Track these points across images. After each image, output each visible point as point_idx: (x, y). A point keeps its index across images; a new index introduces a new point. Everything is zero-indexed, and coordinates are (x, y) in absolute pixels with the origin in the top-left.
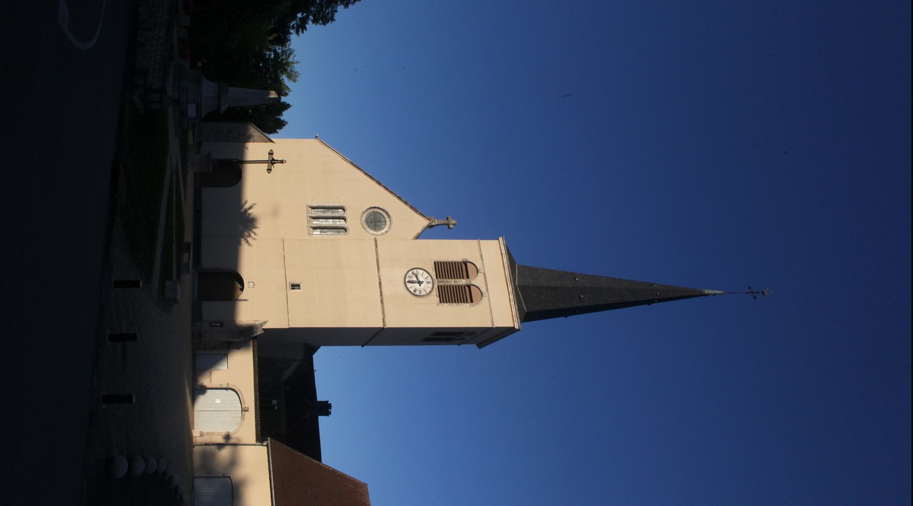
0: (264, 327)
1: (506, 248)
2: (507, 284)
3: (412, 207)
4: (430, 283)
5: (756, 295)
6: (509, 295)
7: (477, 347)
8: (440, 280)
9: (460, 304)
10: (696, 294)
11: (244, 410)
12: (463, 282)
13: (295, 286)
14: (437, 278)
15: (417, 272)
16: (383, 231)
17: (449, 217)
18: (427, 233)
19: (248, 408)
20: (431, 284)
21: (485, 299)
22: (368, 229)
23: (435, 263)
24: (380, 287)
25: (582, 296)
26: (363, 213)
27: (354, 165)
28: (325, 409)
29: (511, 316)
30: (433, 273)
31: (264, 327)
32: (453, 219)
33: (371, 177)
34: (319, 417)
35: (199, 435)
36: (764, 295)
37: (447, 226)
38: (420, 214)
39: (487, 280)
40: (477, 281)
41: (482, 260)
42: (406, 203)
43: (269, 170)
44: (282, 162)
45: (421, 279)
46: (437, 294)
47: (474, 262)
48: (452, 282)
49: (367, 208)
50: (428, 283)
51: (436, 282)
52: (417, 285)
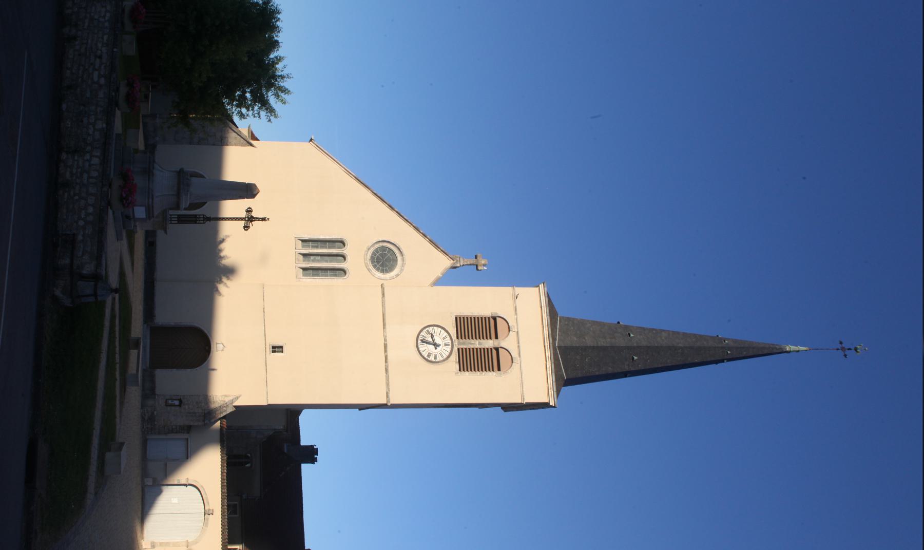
0: (234, 404)
1: (547, 298)
2: (545, 347)
3: (431, 241)
4: (449, 345)
5: (847, 352)
6: (546, 361)
7: (501, 410)
8: (461, 341)
9: (484, 373)
10: (775, 351)
11: (207, 513)
12: (489, 343)
13: (277, 349)
14: (458, 338)
15: (433, 330)
16: (393, 274)
17: (479, 255)
18: (449, 278)
19: (213, 510)
20: (450, 346)
21: (516, 366)
22: (374, 271)
23: (456, 318)
24: (386, 351)
25: (635, 358)
26: (369, 249)
27: (360, 181)
28: (310, 454)
29: (546, 388)
30: (453, 332)
31: (236, 404)
32: (483, 258)
33: (381, 199)
34: (303, 465)
35: (150, 547)
36: (857, 352)
37: (475, 266)
38: (442, 250)
39: (520, 342)
40: (507, 342)
41: (516, 314)
42: (424, 236)
43: (246, 228)
44: (264, 219)
45: (438, 340)
46: (456, 359)
47: (505, 318)
48: (476, 344)
49: (375, 242)
50: (446, 345)
51: (457, 344)
52: (432, 347)
